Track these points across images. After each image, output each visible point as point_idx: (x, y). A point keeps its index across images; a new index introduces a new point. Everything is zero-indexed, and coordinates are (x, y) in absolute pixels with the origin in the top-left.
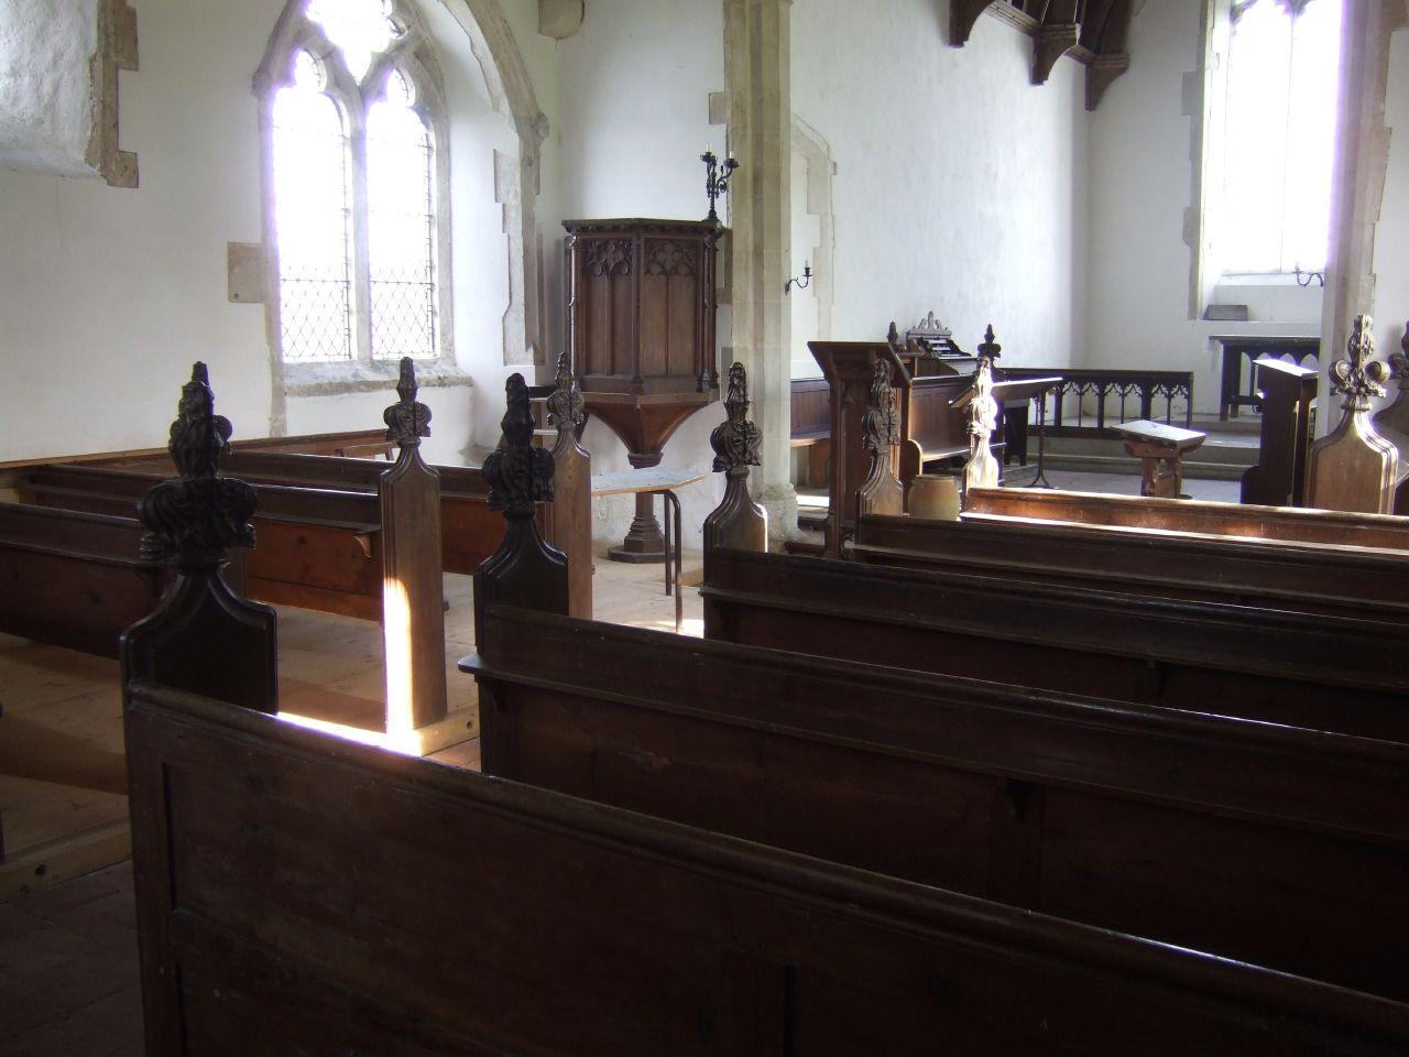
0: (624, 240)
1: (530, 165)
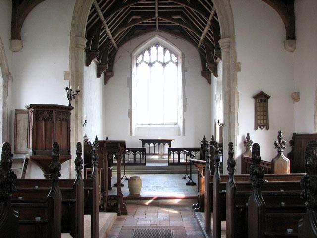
0: (50, 111)
1: (6, 87)
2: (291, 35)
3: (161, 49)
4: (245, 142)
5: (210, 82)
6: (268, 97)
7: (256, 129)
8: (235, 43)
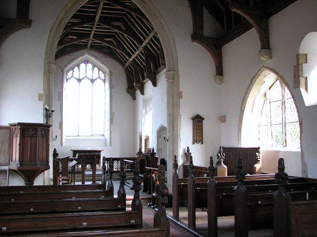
2: (220, 72)
3: (90, 66)
4: (186, 154)
5: (134, 98)
6: (203, 119)
7: (194, 143)
8: (178, 76)
